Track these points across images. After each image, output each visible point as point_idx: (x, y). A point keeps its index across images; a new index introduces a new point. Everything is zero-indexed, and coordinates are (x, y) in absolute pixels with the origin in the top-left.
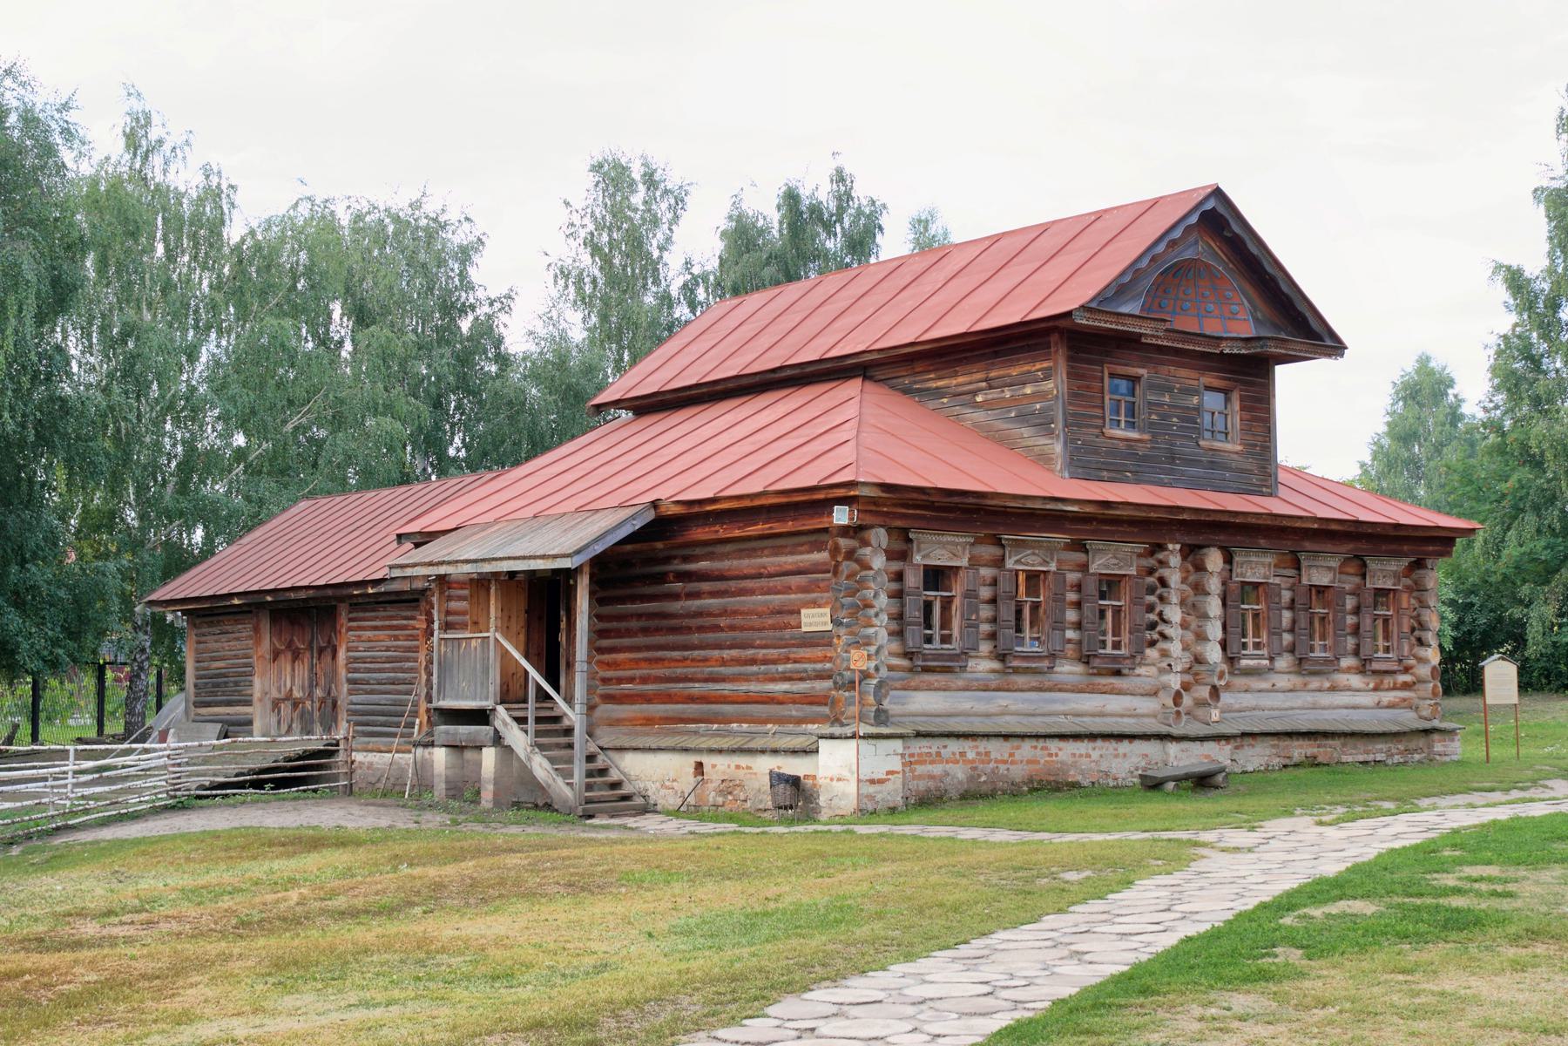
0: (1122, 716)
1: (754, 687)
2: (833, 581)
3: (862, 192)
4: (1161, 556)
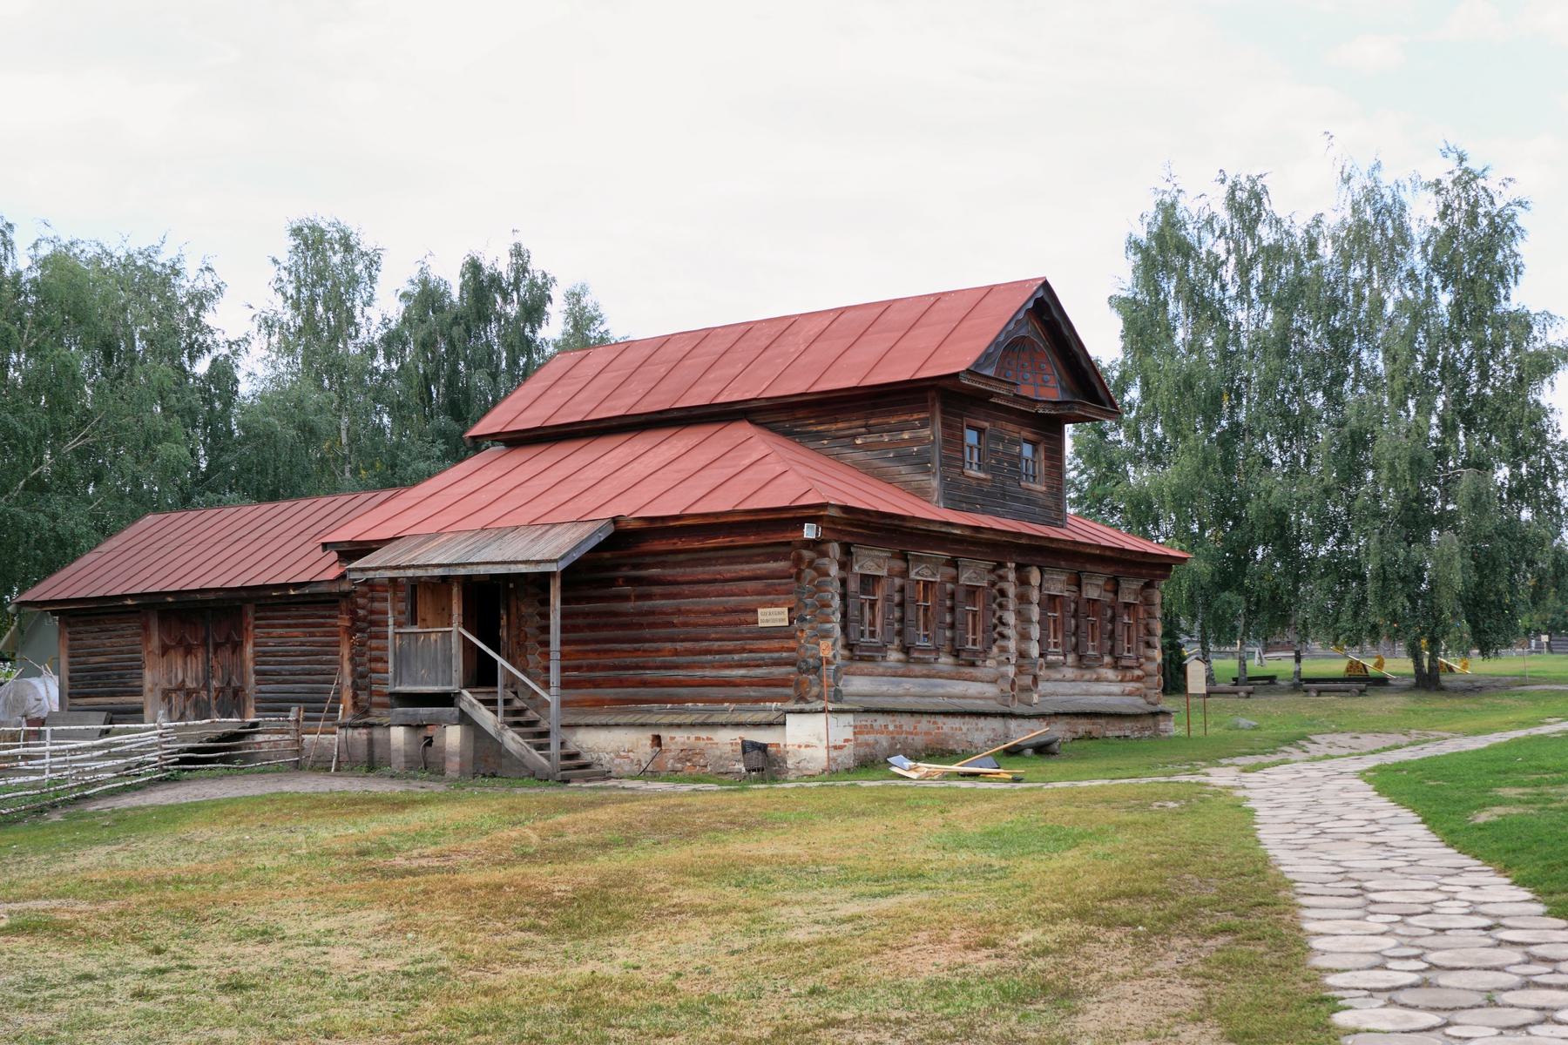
0: (976, 698)
1: (708, 673)
2: (796, 585)
3: (536, 266)
4: (1001, 572)
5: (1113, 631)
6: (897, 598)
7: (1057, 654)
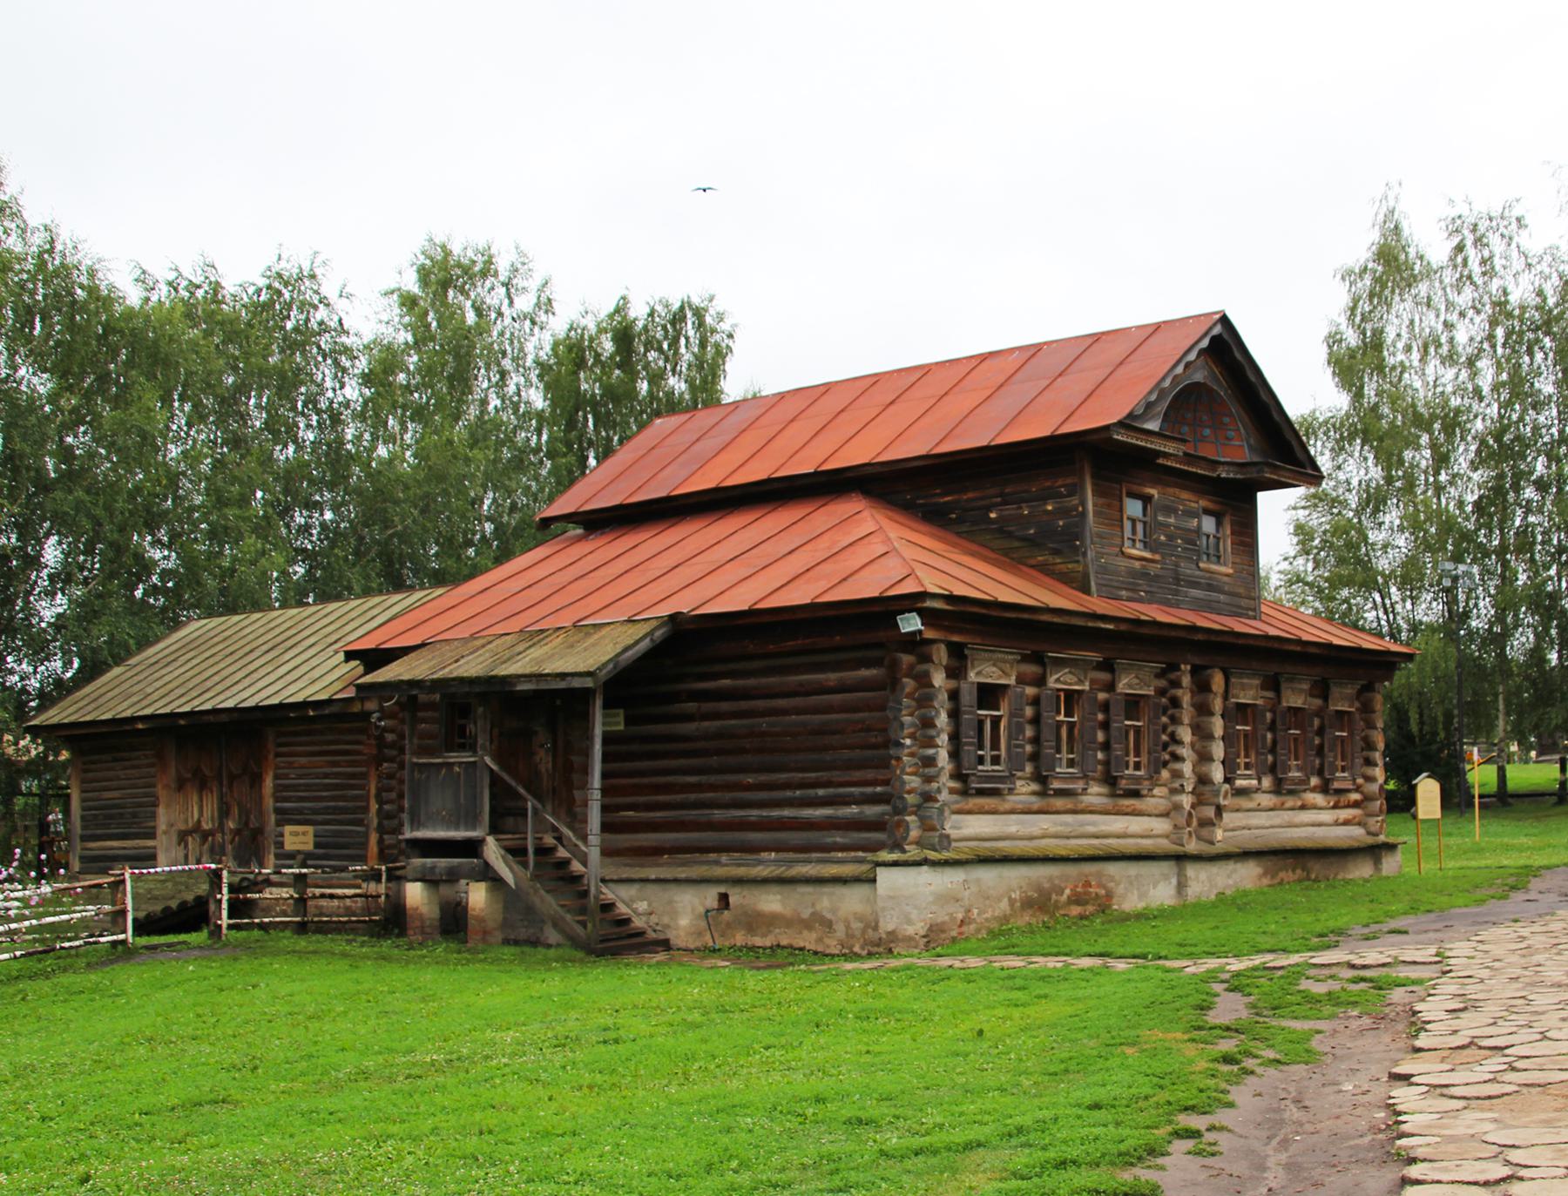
4: (1172, 676)
5: (1321, 747)
6: (1029, 711)
7: (1249, 777)
